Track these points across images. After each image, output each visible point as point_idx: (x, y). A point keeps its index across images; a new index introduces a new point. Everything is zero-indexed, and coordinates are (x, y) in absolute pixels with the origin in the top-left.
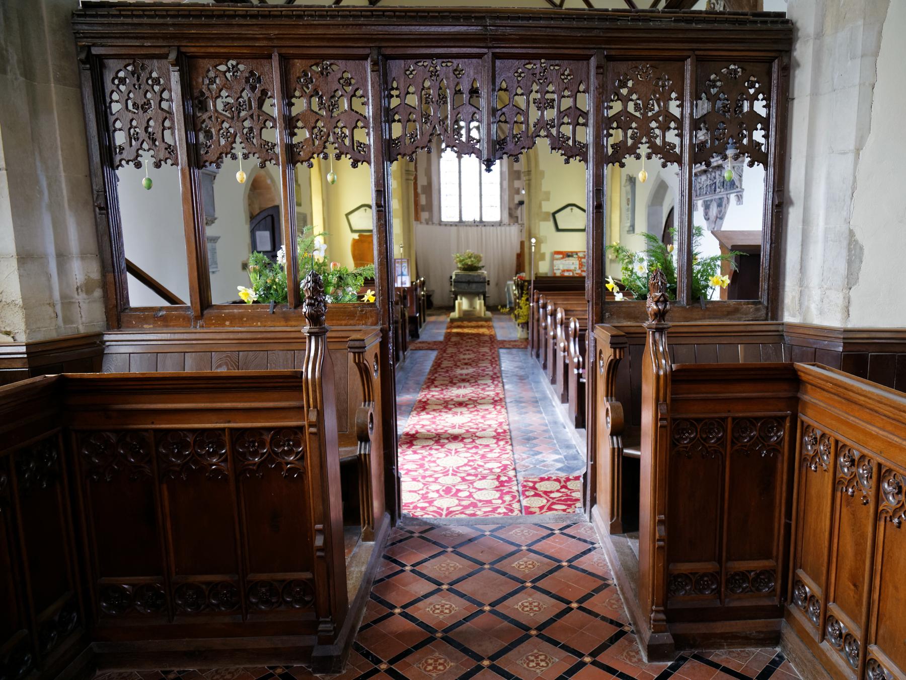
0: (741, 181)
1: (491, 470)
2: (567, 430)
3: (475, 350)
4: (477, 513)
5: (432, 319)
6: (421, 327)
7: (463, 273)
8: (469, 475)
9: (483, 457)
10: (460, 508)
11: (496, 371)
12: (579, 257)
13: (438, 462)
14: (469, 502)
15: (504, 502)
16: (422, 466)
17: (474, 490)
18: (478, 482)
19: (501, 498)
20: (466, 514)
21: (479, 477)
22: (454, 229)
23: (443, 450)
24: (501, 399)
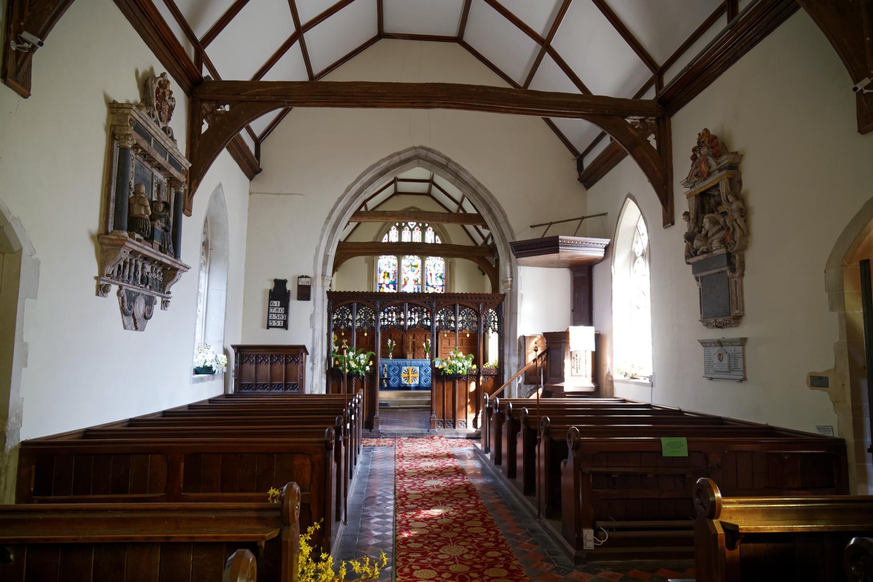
2: (361, 461)
15: (410, 567)
17: (428, 528)
19: (412, 570)
20: (439, 559)
21: (426, 536)
24: (399, 474)
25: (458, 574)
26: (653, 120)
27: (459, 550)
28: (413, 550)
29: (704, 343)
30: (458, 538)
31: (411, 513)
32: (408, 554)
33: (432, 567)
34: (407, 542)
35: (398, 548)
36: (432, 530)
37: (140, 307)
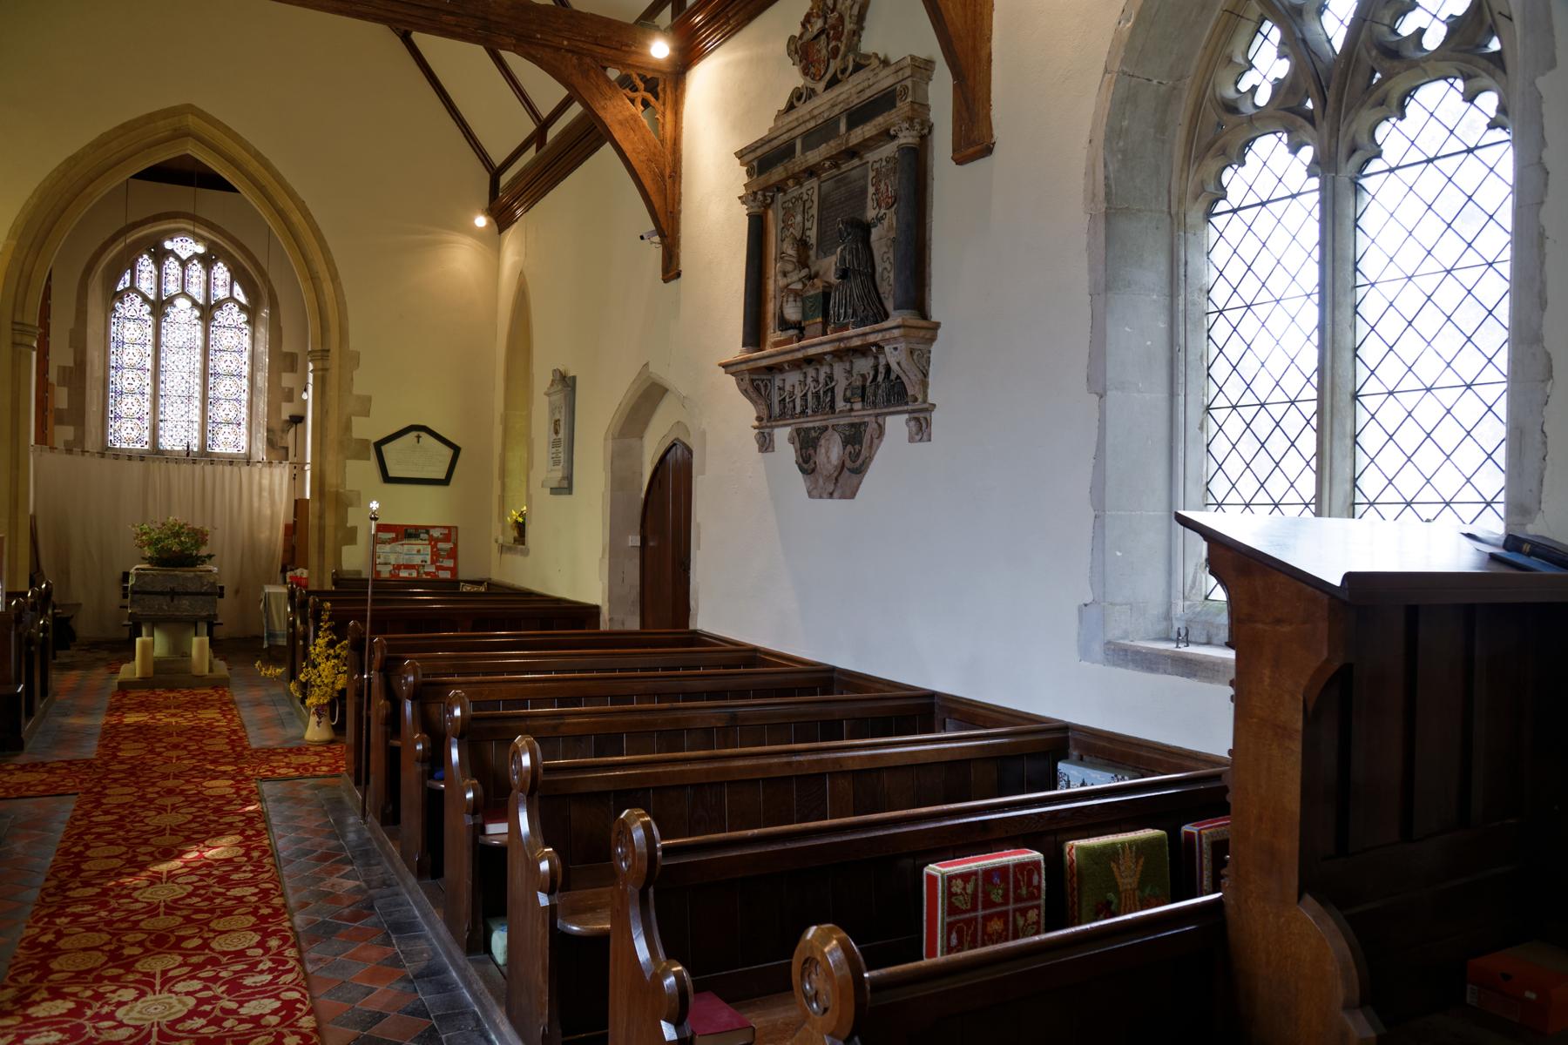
0: (924, 384)
1: (256, 1020)
3: (191, 789)
4: (221, 975)
5: (72, 677)
6: (30, 713)
7: (157, 571)
8: (195, 833)
9: (234, 986)
10: (186, 970)
11: (234, 726)
13: (120, 1014)
15: (267, 950)
17: (212, 935)
18: (216, 921)
20: (199, 979)
21: (218, 912)
22: (137, 466)
23: (131, 977)
25: (168, 949)
27: (140, 1012)
28: (265, 992)
31: (242, 875)
32: (276, 978)
33: (220, 957)
34: (261, 895)
35: (303, 991)
36: (201, 930)
37: (832, 452)
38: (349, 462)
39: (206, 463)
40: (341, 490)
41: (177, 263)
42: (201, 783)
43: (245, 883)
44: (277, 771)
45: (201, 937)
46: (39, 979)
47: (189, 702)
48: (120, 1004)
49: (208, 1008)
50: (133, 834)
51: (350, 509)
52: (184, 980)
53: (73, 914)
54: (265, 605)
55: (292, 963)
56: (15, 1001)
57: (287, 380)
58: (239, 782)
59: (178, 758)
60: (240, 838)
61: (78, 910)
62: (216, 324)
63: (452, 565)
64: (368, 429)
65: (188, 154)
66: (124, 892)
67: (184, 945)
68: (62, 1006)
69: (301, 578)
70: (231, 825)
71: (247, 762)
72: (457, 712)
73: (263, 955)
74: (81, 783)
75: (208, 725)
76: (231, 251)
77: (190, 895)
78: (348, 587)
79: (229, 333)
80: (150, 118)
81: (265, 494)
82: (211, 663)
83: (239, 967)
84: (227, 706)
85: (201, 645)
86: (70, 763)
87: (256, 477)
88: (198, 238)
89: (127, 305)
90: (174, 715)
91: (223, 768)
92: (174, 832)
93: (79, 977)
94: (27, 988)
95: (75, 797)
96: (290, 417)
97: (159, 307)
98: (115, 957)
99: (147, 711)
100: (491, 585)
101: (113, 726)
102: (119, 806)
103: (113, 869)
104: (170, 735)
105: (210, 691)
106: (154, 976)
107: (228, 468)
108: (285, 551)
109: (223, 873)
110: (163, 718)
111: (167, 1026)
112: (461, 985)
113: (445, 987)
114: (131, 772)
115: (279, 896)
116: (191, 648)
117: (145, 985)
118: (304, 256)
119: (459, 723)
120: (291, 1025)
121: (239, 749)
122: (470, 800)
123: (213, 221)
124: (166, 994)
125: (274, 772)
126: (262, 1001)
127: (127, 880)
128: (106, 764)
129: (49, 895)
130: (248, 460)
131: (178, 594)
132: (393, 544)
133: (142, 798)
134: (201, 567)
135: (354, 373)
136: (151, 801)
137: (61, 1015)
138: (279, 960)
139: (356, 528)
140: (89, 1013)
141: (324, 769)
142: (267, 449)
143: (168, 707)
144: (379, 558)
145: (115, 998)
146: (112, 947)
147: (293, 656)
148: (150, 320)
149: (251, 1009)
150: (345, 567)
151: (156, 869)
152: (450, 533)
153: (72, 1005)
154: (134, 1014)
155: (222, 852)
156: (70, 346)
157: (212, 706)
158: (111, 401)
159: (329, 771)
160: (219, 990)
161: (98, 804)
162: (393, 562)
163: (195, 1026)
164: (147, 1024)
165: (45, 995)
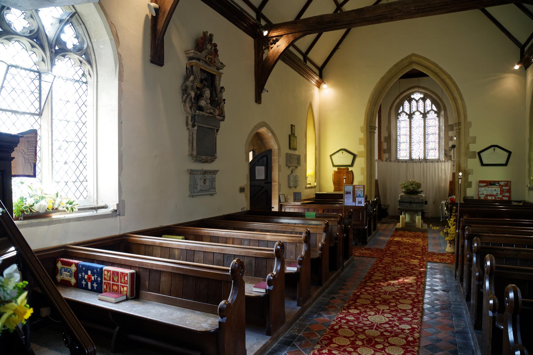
1: (403, 330)
3: (406, 261)
4: (398, 315)
7: (406, 196)
9: (400, 319)
10: (389, 311)
11: (425, 244)
12: (500, 185)
14: (394, 309)
15: (412, 311)
16: (358, 319)
17: (399, 303)
20: (392, 314)
21: (403, 298)
22: (404, 164)
23: (374, 309)
26: (445, 165)
27: (374, 319)
28: (408, 323)
29: (192, 172)
30: (368, 328)
31: (413, 289)
32: (412, 320)
33: (399, 310)
35: (419, 326)
36: (396, 301)
38: (468, 159)
39: (424, 162)
40: (466, 169)
41: (415, 102)
42: (410, 260)
43: (413, 291)
44: (434, 260)
45: (395, 303)
46: (353, 303)
47: (414, 236)
48: (370, 315)
49: (391, 323)
50: (387, 271)
51: (469, 176)
52: (387, 314)
53: (366, 289)
54: (441, 207)
55: (418, 317)
56: (347, 307)
57: (451, 134)
58: (421, 261)
59: (406, 252)
60: (416, 278)
61: (367, 288)
62: (428, 118)
63: (509, 195)
64: (475, 148)
65: (414, 69)
66: (380, 286)
67: (390, 304)
68: (357, 311)
69: (453, 199)
70: (414, 273)
71: (425, 256)
72: (476, 245)
73: (411, 313)
74: (378, 255)
75: (417, 243)
76: (431, 95)
77: (396, 291)
78: (468, 201)
79: (431, 121)
80: (402, 61)
81: (443, 171)
82: (422, 224)
83: (403, 314)
84: (425, 238)
85: (419, 219)
86: (377, 249)
87: (440, 166)
88: (421, 93)
89: (401, 116)
90: (408, 239)
91: (417, 257)
92: (398, 272)
93: (362, 305)
94: (350, 305)
95: (376, 259)
96: (452, 146)
97: (410, 116)
98: (372, 303)
99: (401, 237)
100: (525, 203)
101: (391, 241)
102: (386, 263)
103: (379, 280)
104: (405, 245)
105: (421, 233)
106: (380, 310)
107: (431, 164)
108: (450, 190)
109: (407, 287)
110: (405, 240)
111: (379, 324)
112: (471, 339)
113: (466, 338)
114: (392, 254)
115: (422, 297)
116: (416, 220)
117: (377, 312)
118: (451, 92)
119: (476, 249)
120: (412, 334)
121: (424, 251)
122: (477, 276)
123: (425, 87)
124: (382, 316)
125: (432, 260)
126: (406, 325)
127: (382, 284)
128: (386, 251)
129: (362, 283)
130: (438, 161)
131: (412, 203)
132: (485, 188)
133: (392, 262)
134: (419, 195)
135: (470, 129)
136: (395, 263)
137: (356, 314)
138: (415, 315)
139: (472, 182)
140: (362, 315)
141: (449, 261)
142: (445, 157)
143: (407, 237)
144: (480, 192)
145: (369, 313)
146: (372, 300)
147: (444, 224)
148: (408, 120)
149: (402, 326)
150: (468, 195)
151: (390, 282)
152: (508, 183)
153: (359, 312)
154: (372, 319)
155: (410, 281)
156: (387, 130)
157: (420, 238)
158: (398, 145)
159: (450, 262)
160: (396, 319)
161: (381, 261)
162: (485, 194)
163: (386, 326)
164: (375, 322)
165: (354, 307)
